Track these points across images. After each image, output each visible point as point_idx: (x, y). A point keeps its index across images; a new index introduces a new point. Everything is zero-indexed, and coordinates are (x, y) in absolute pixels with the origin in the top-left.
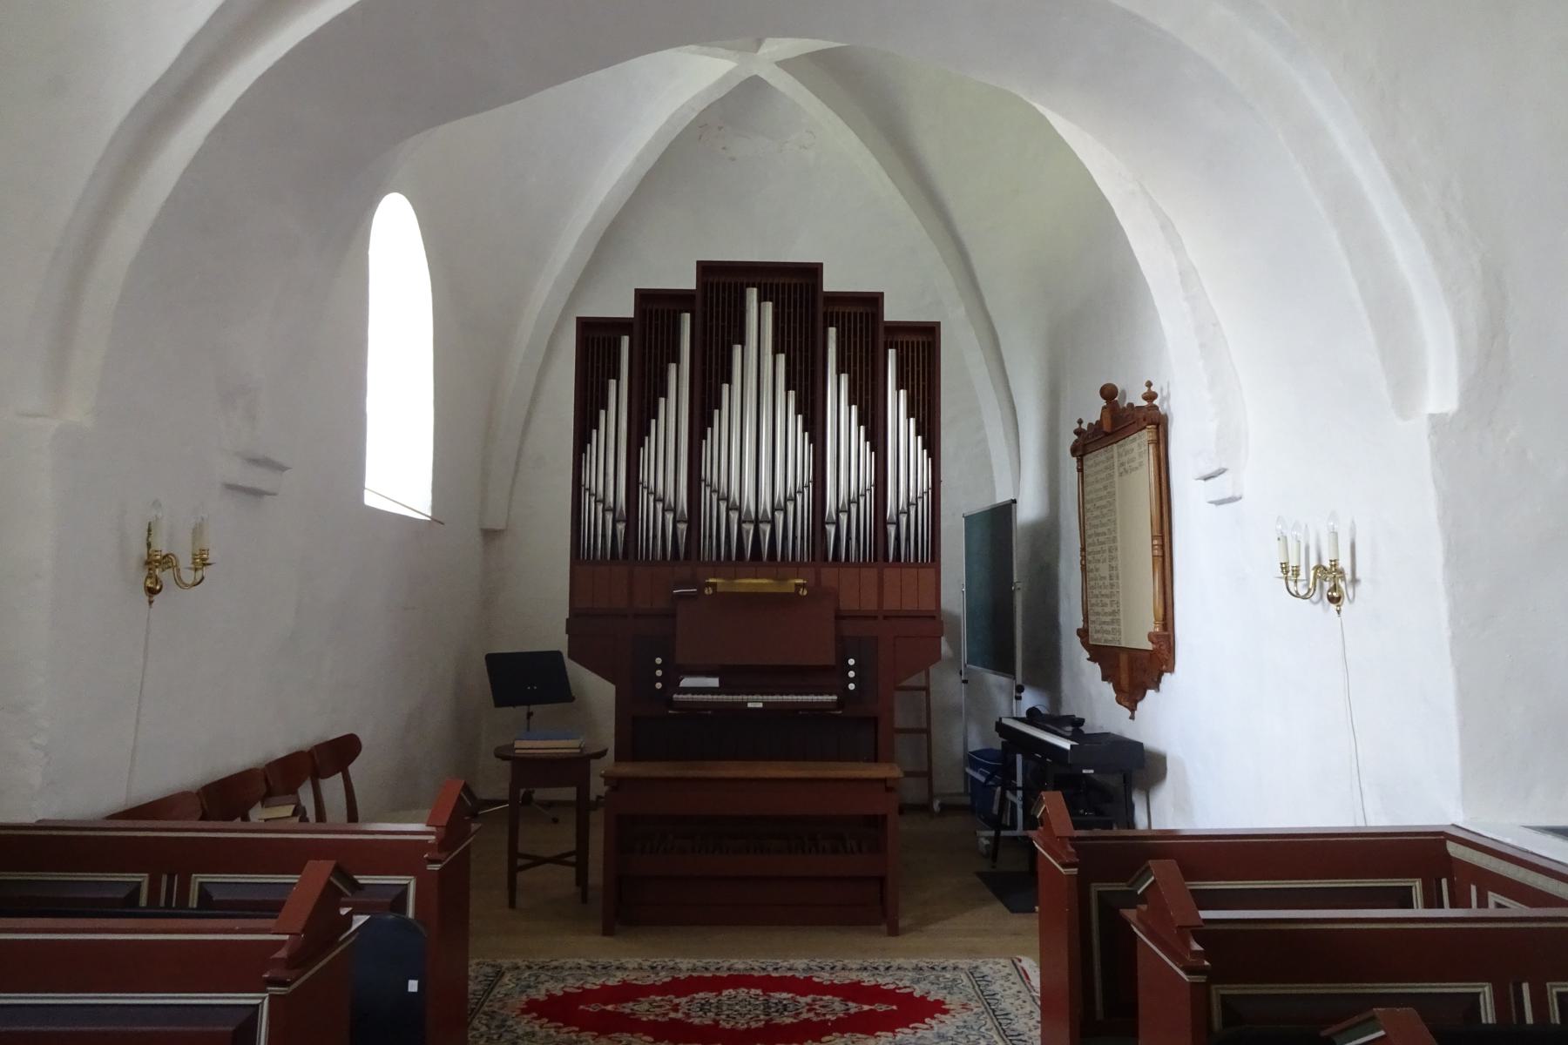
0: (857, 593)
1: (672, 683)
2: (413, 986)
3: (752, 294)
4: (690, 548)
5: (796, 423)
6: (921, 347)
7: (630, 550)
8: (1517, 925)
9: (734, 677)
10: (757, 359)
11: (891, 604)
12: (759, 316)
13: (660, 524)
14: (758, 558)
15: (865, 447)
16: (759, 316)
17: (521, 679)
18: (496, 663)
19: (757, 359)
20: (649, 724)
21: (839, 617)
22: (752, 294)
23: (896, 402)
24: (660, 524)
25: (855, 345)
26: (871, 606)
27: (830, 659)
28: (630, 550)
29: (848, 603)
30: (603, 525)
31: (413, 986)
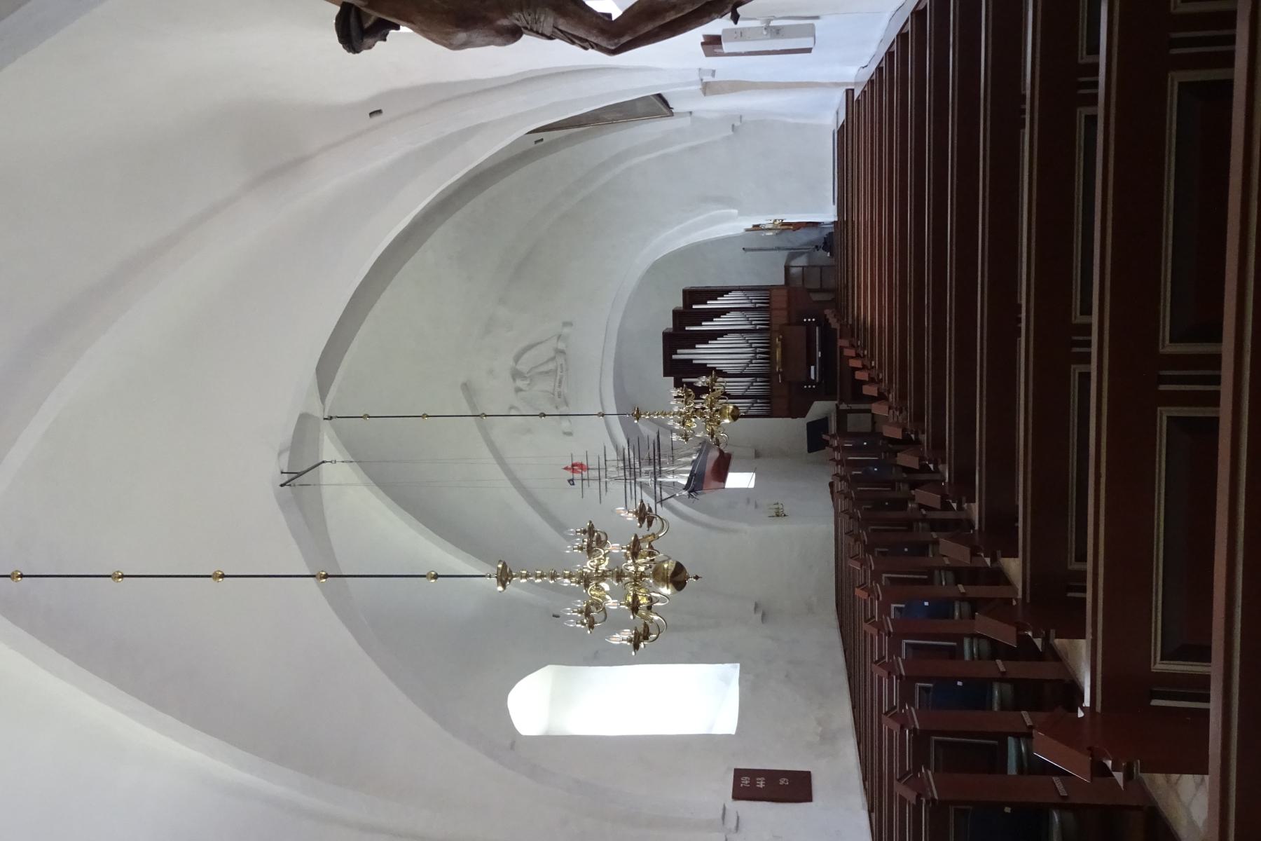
0: (780, 318)
1: (813, 382)
2: (926, 604)
3: (674, 357)
4: (767, 376)
5: (712, 344)
6: (693, 295)
7: (766, 398)
8: (1237, 662)
9: (811, 361)
10: (703, 354)
11: (785, 306)
12: (683, 354)
13: (758, 387)
14: (769, 354)
15: (728, 315)
16: (683, 354)
17: (817, 437)
18: (810, 450)
19: (703, 354)
20: (824, 391)
21: (789, 324)
22: (674, 357)
23: (711, 304)
24: (758, 387)
25: (690, 320)
26: (785, 313)
27: (803, 329)
28: (766, 398)
29: (785, 321)
30: (758, 407)
31: (926, 604)
